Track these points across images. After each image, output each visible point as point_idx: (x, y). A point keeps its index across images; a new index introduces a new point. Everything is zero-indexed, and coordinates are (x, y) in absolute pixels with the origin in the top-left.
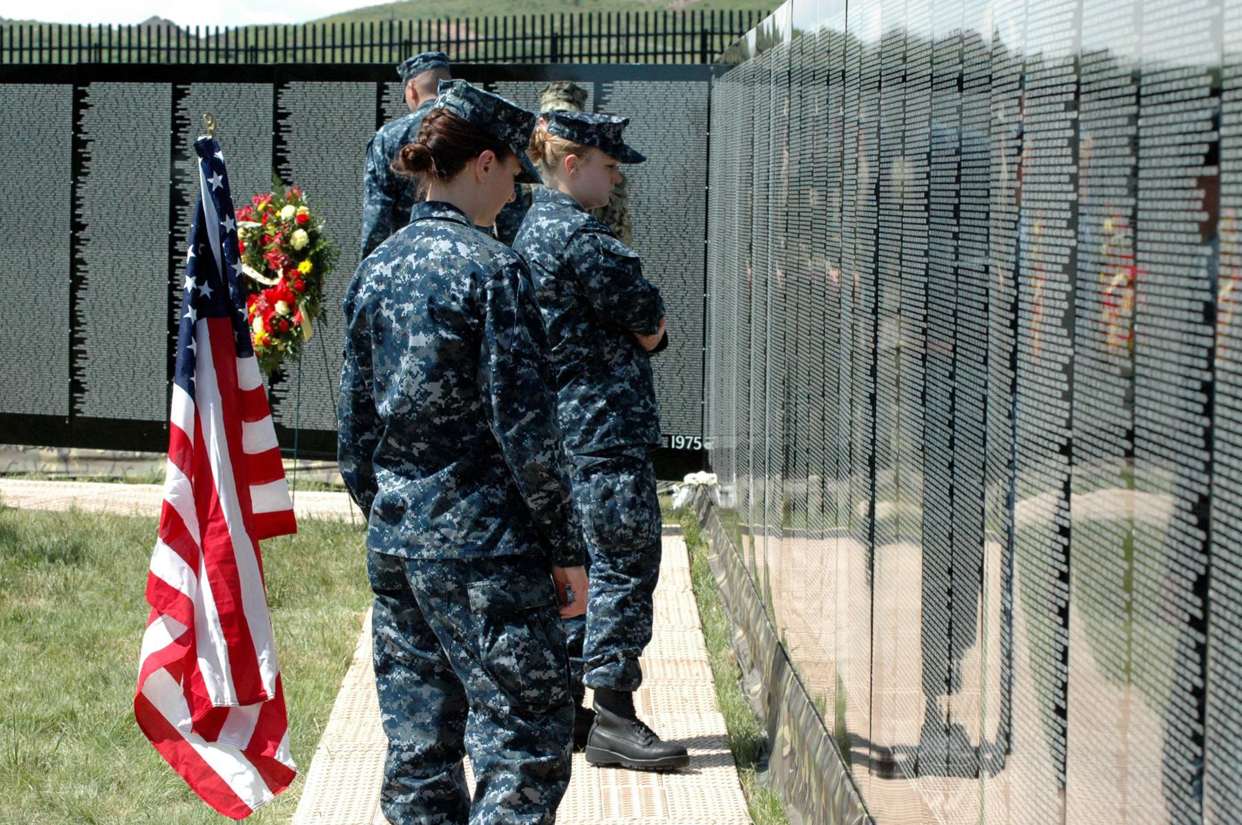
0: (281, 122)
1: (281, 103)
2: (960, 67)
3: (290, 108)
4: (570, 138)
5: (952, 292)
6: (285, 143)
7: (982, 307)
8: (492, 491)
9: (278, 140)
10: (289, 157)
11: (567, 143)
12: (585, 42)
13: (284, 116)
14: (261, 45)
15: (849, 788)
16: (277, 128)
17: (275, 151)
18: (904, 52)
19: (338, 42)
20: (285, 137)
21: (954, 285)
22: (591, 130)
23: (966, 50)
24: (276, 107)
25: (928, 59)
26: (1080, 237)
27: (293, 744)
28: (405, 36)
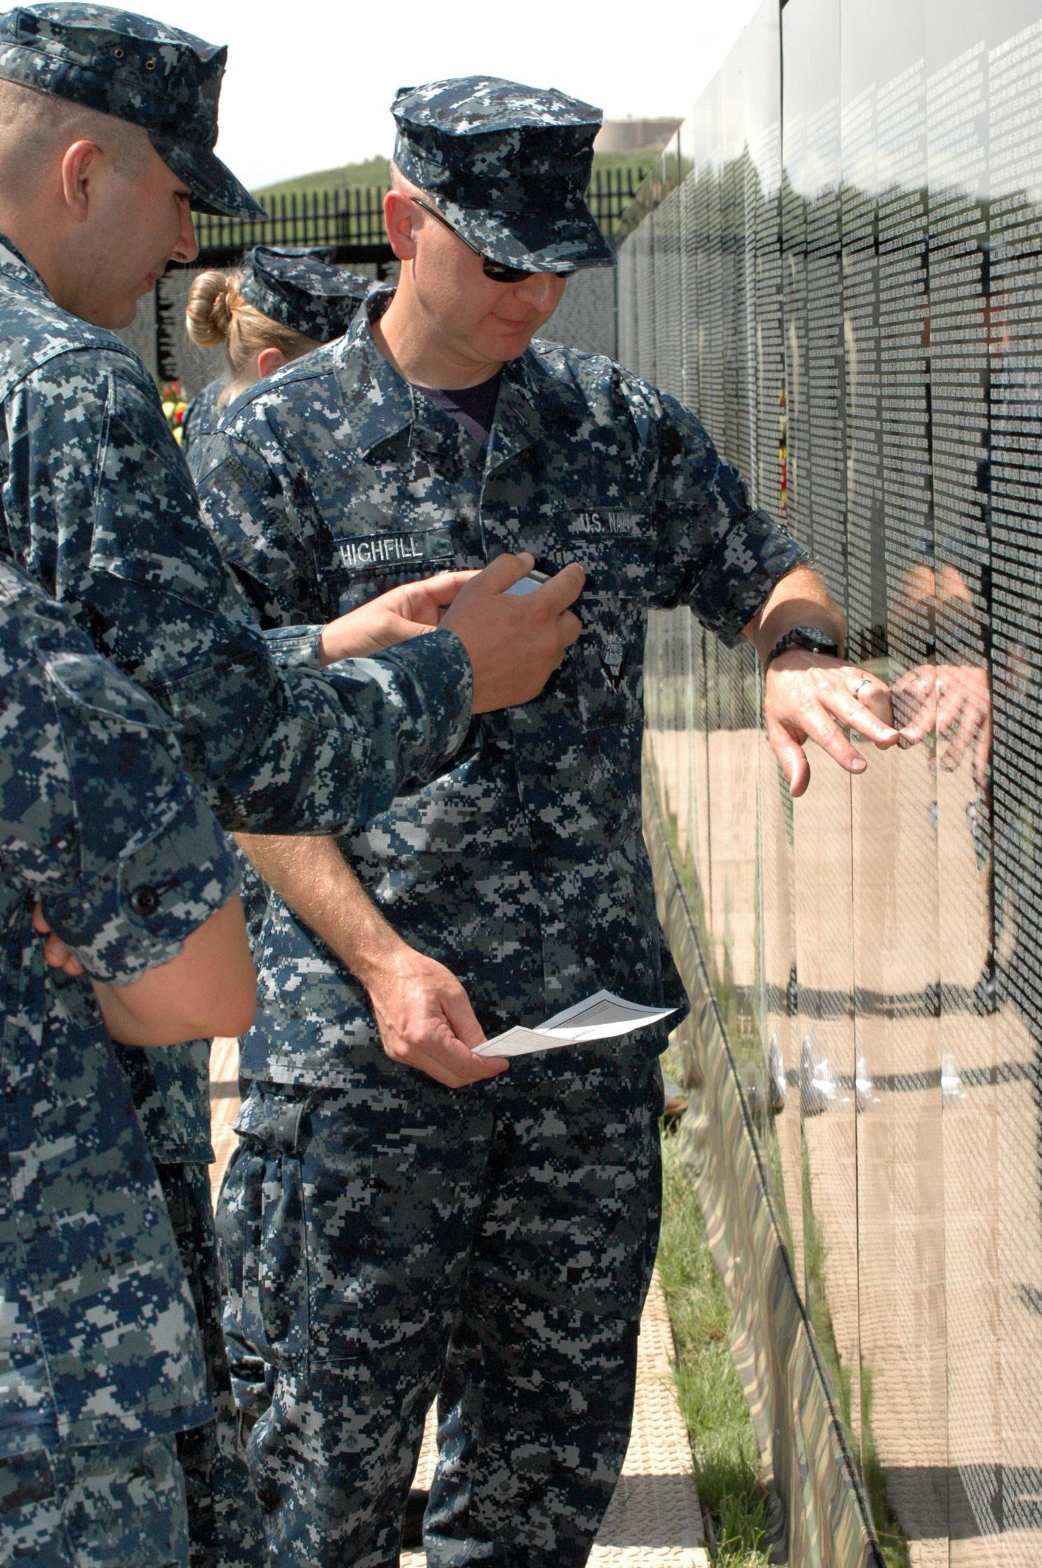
0: (164, 314)
1: (163, 294)
2: (923, 221)
3: (173, 298)
4: (275, 314)
5: (873, 470)
6: (168, 336)
7: (922, 482)
8: (189, 646)
9: (161, 334)
10: (173, 351)
11: (269, 324)
12: (311, 224)
13: (167, 307)
14: (353, 209)
15: (700, 974)
16: (160, 320)
17: (159, 344)
18: (839, 211)
19: (289, 214)
20: (169, 329)
21: (876, 460)
22: (313, 307)
23: (845, 208)
24: (158, 298)
25: (834, 217)
26: (805, 389)
27: (666, 1277)
28: (342, 207)
